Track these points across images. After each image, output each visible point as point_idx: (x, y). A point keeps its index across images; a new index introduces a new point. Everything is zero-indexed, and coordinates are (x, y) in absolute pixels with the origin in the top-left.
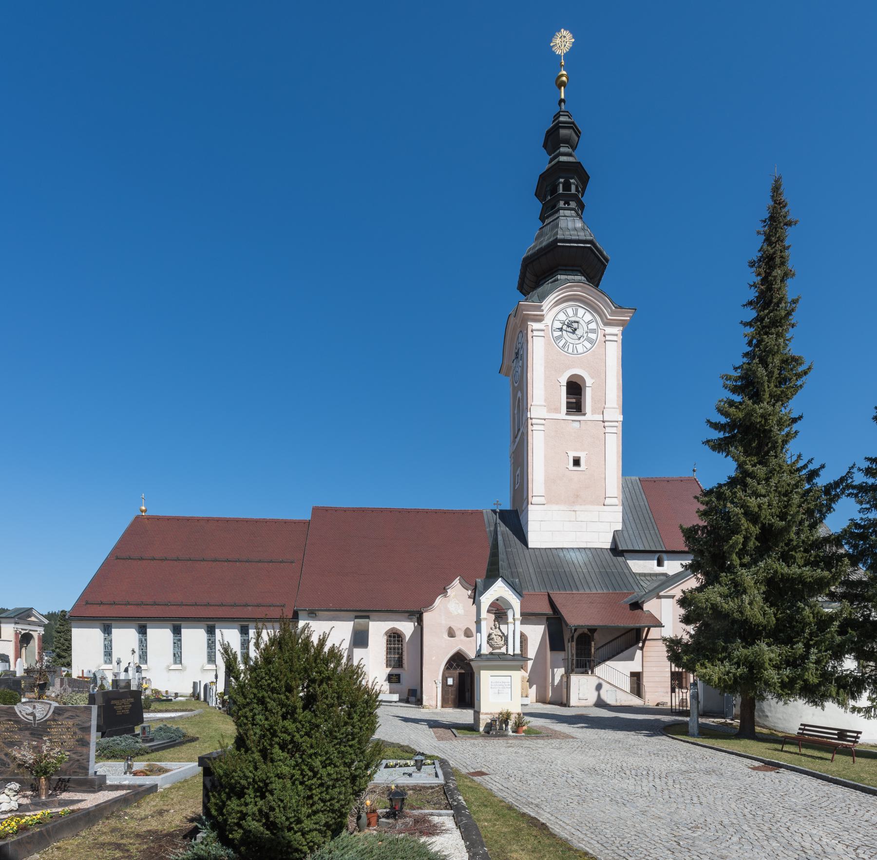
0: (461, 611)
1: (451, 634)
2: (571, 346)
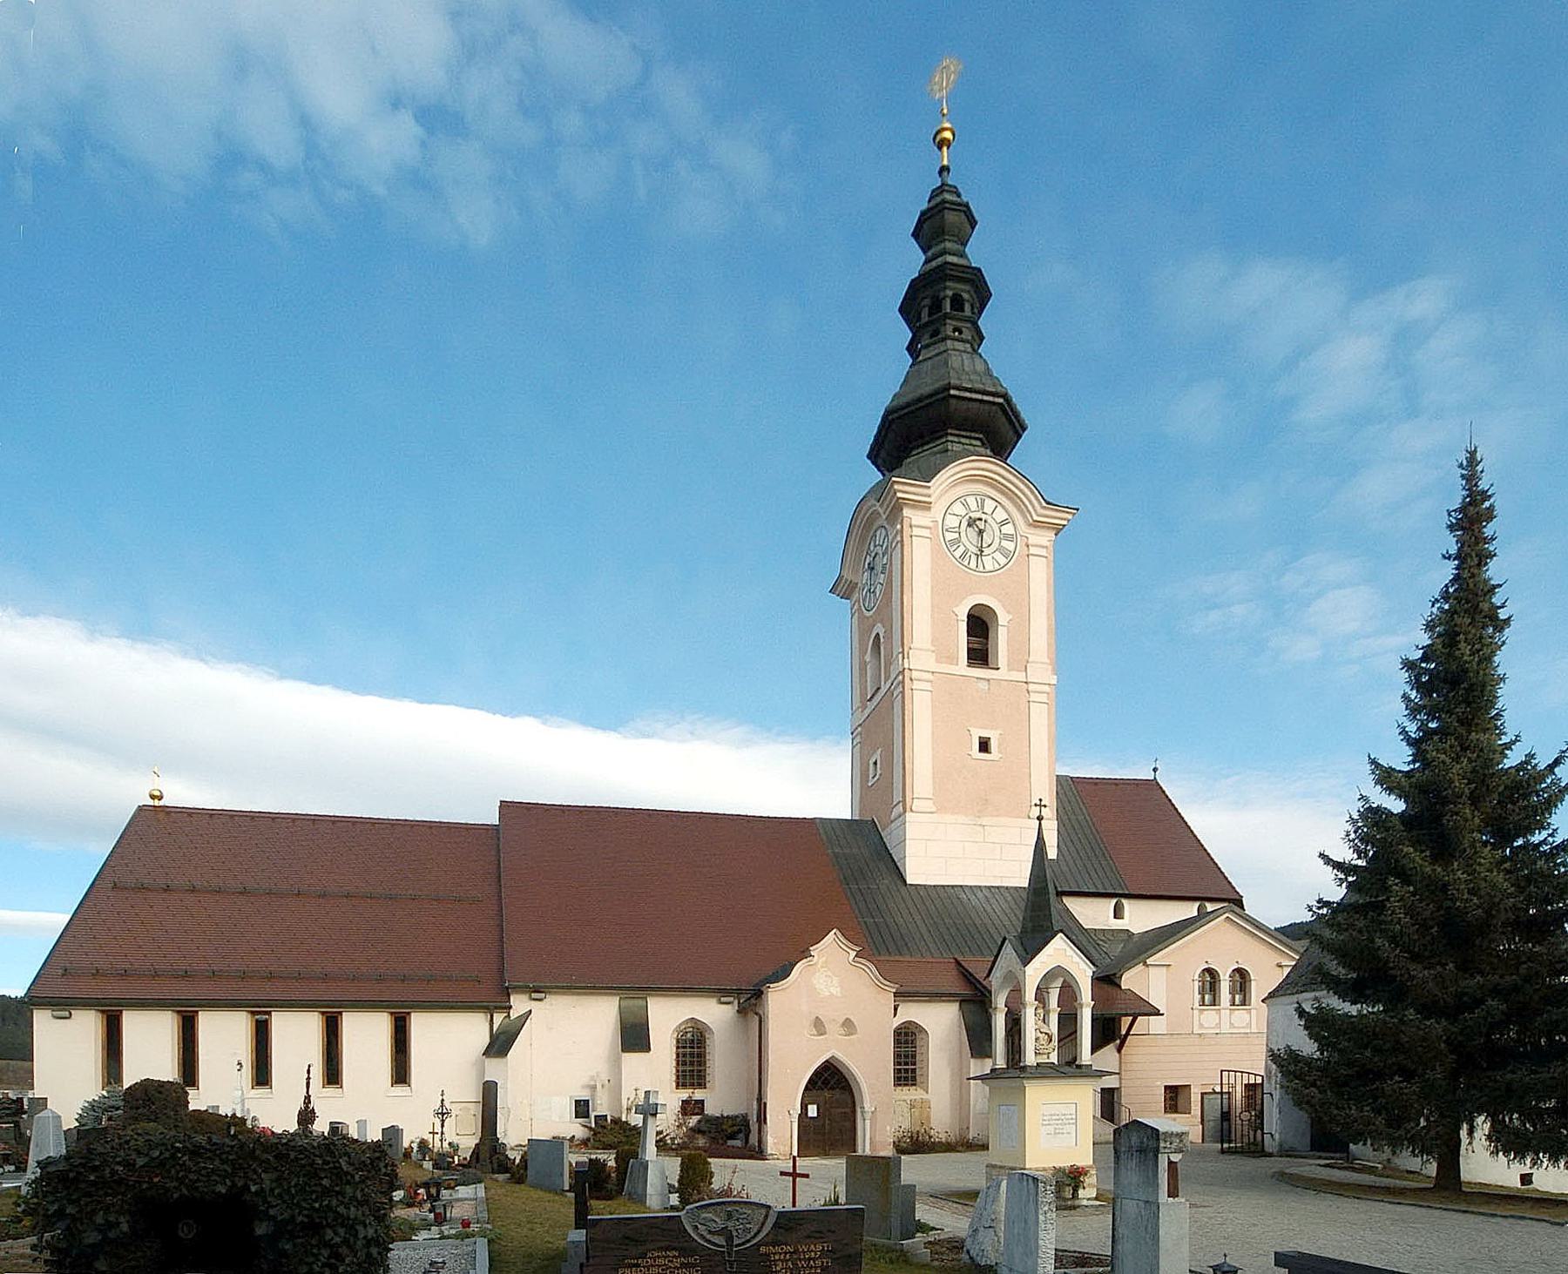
0: (836, 991)
1: (819, 1026)
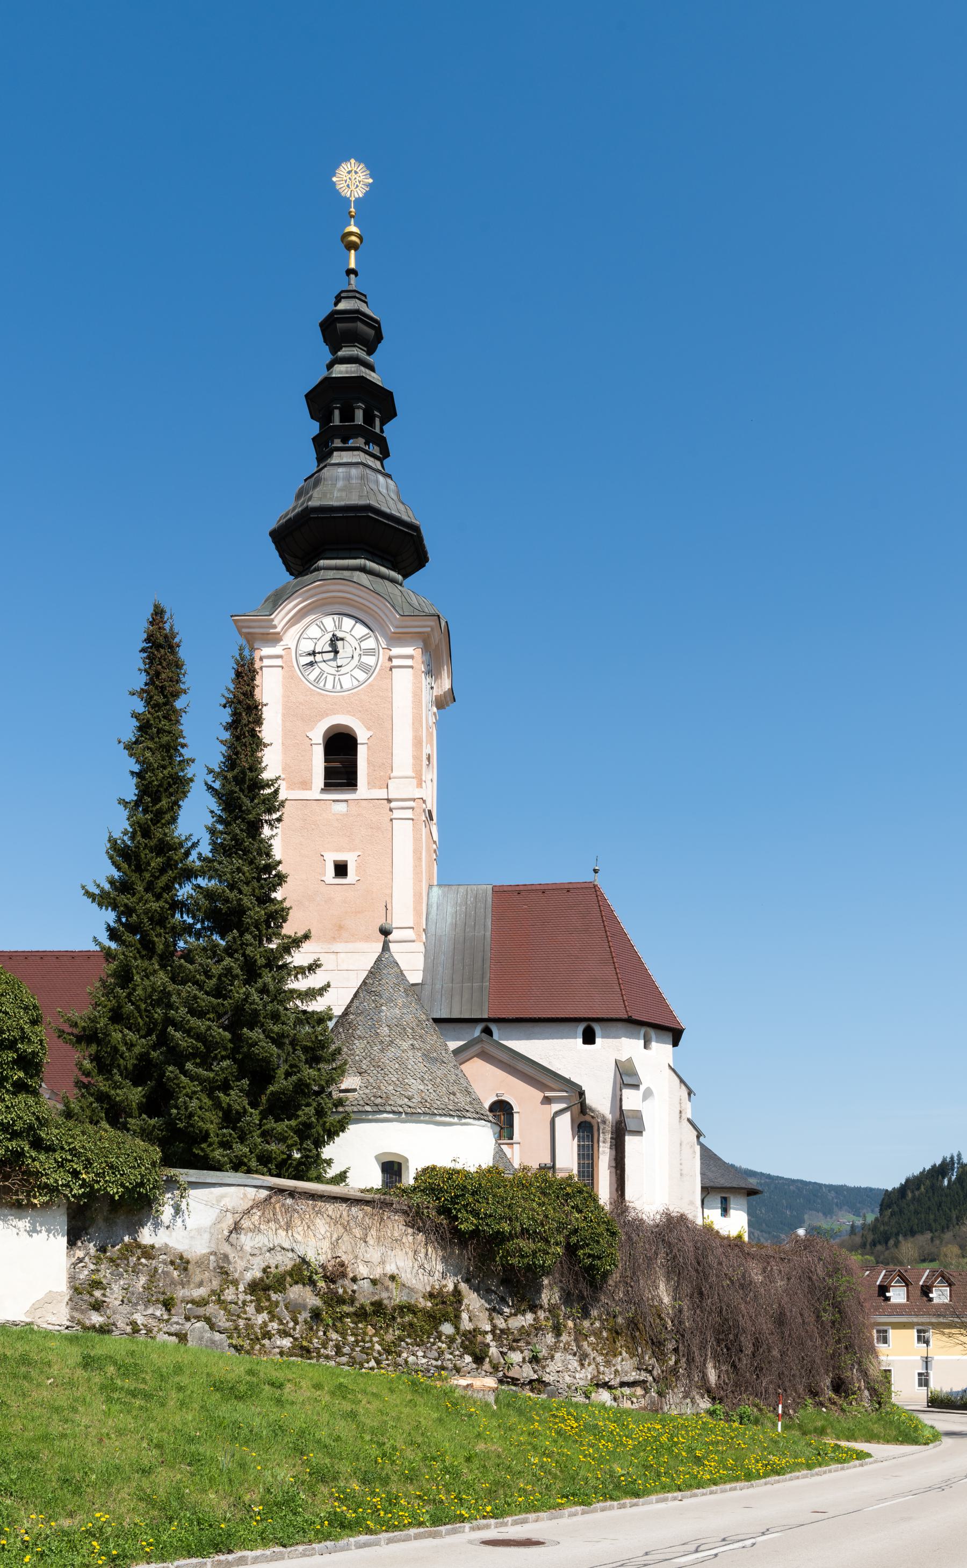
2: (330, 678)
